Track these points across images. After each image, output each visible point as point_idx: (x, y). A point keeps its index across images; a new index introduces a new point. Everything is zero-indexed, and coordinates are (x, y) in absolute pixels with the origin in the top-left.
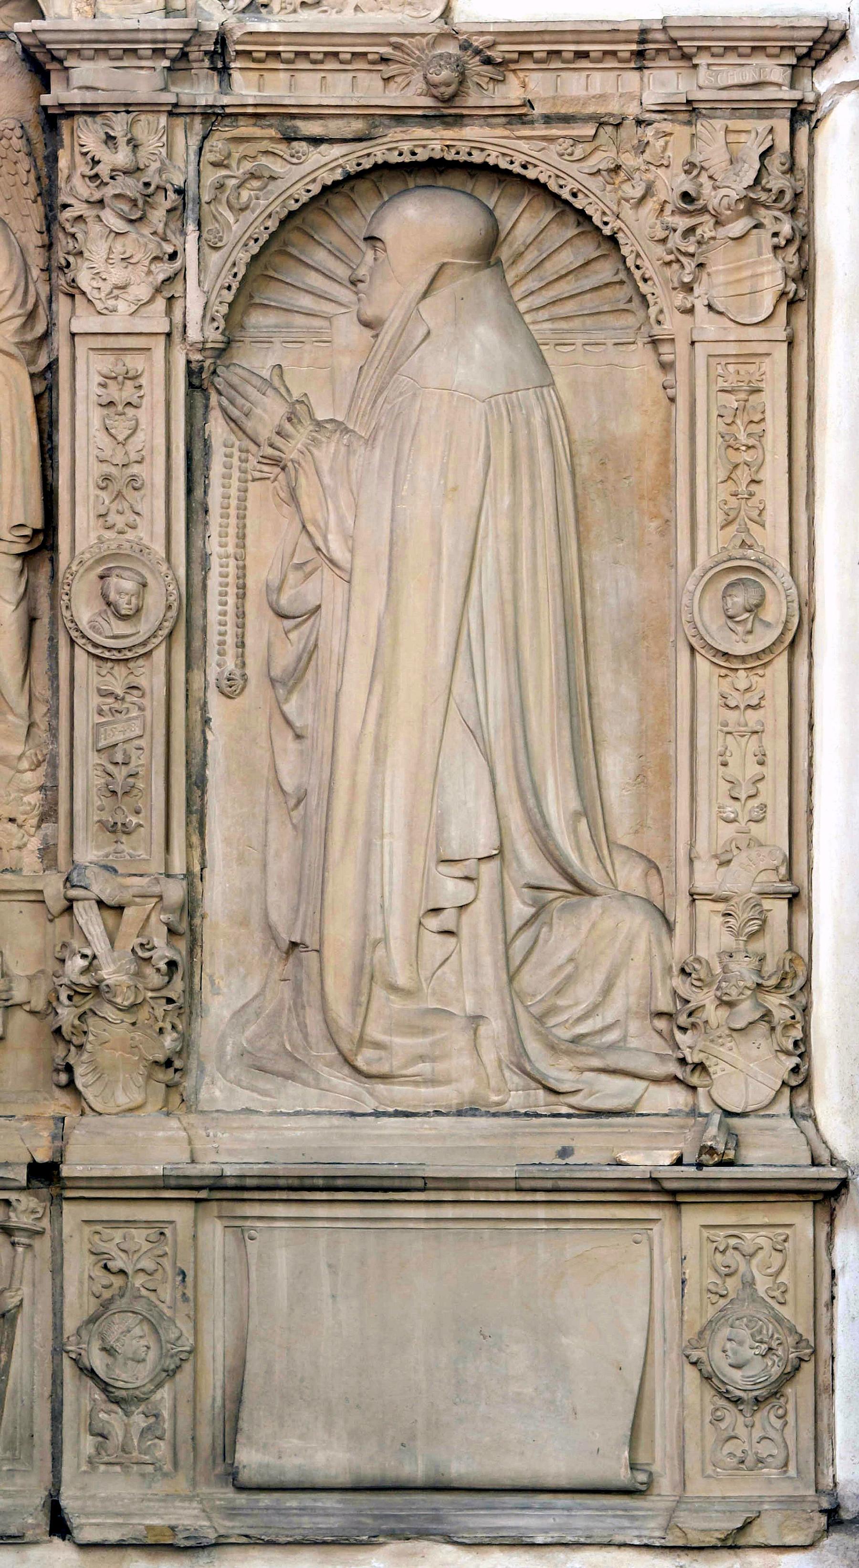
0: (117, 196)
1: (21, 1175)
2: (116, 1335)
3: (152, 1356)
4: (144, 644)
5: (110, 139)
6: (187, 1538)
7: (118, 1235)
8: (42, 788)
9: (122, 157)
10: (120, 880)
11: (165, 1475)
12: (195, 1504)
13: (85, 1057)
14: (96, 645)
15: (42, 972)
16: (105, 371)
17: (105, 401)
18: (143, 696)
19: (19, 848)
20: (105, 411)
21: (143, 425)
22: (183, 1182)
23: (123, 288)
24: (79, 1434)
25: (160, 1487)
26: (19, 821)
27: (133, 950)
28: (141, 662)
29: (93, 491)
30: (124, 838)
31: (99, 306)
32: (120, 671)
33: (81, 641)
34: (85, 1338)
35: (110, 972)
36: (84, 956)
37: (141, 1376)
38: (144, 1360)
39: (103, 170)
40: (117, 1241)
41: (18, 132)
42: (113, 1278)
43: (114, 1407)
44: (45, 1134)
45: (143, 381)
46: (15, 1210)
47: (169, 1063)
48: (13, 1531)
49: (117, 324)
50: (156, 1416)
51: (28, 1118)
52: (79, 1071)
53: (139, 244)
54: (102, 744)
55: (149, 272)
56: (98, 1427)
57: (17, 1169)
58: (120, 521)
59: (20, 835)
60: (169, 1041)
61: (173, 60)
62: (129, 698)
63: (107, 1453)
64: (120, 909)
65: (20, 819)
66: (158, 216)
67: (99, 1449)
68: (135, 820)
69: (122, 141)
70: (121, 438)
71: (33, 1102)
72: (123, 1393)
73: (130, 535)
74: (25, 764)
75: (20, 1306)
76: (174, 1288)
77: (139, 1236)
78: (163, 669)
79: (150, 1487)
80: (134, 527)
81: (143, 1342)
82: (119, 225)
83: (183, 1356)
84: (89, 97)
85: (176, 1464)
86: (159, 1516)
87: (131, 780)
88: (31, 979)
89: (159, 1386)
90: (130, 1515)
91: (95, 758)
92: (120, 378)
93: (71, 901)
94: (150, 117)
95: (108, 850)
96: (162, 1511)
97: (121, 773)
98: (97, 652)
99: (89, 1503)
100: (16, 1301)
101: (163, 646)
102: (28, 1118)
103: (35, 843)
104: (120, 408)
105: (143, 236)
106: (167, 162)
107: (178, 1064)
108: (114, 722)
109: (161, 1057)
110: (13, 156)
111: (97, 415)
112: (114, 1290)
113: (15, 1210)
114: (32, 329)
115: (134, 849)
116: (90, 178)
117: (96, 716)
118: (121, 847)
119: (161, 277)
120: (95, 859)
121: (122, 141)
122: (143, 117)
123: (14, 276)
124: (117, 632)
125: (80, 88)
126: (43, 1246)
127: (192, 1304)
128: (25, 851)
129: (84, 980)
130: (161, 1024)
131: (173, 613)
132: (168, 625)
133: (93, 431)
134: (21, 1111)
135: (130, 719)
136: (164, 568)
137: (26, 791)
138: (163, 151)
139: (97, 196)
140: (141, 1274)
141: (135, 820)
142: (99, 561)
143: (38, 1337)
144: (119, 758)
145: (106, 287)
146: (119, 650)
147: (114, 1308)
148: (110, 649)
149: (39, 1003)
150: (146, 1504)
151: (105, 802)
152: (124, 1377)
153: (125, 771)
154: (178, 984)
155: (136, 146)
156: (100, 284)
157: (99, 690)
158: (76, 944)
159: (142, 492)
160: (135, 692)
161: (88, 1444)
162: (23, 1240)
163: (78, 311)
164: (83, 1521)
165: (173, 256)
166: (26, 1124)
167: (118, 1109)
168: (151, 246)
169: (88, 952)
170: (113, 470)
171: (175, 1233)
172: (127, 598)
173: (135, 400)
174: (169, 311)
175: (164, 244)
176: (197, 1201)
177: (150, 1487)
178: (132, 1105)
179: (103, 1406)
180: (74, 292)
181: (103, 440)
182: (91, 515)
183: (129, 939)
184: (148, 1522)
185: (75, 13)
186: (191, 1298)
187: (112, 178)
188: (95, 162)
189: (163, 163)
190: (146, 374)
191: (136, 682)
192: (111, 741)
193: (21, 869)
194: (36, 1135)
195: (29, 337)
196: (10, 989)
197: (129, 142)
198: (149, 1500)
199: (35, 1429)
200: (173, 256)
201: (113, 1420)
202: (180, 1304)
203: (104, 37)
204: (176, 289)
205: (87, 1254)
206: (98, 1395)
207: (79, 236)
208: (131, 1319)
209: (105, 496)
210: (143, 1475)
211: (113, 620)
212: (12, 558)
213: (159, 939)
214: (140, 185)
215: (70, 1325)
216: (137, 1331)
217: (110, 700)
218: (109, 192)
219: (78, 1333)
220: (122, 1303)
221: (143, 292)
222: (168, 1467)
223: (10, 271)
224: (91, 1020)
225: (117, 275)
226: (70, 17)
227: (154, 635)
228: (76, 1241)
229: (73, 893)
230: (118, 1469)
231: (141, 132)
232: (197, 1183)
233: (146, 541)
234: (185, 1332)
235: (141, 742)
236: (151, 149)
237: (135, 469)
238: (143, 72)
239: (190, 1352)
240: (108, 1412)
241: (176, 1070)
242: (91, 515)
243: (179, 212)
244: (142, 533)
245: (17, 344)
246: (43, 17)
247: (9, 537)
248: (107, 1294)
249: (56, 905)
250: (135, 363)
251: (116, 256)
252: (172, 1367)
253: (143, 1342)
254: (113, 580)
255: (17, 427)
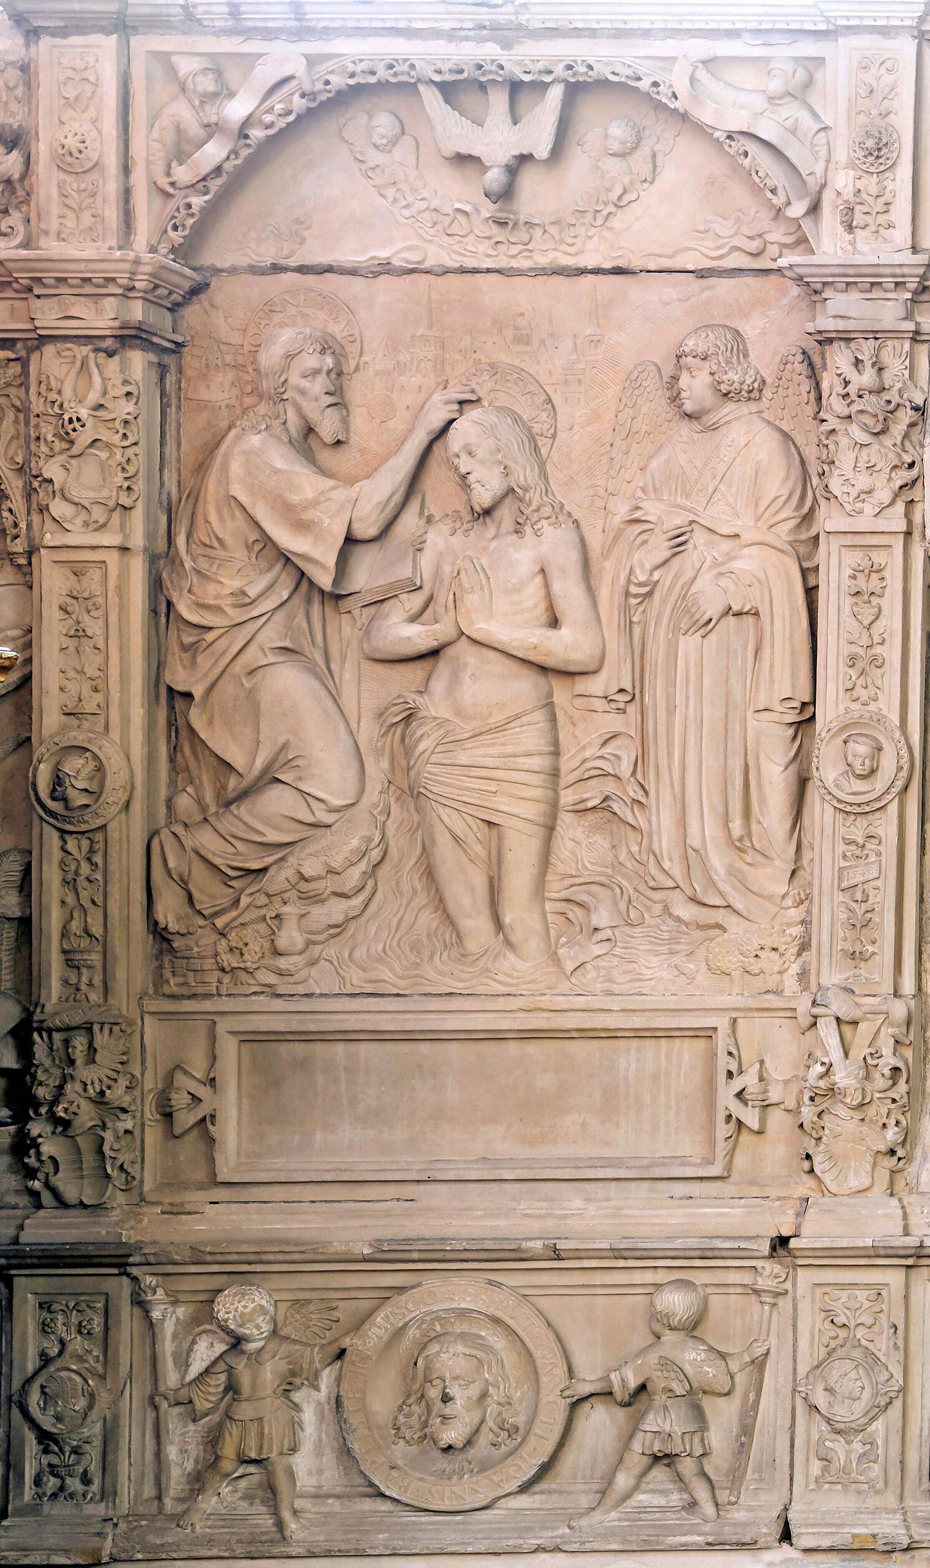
0: (862, 412)
1: (766, 1248)
2: (836, 1378)
3: (866, 1395)
4: (878, 799)
5: (858, 362)
6: (885, 1544)
7: (844, 1295)
8: (802, 922)
9: (867, 378)
10: (856, 999)
11: (877, 1492)
12: (898, 1516)
13: (822, 1147)
14: (839, 801)
15: (795, 1076)
16: (855, 565)
17: (853, 592)
18: (880, 844)
19: (780, 973)
20: (855, 600)
21: (885, 612)
22: (890, 1252)
23: (870, 492)
24: (808, 1459)
25: (873, 1502)
26: (781, 950)
27: (865, 1058)
28: (878, 815)
29: (843, 669)
30: (862, 964)
31: (848, 508)
32: (862, 822)
33: (828, 797)
34: (811, 1380)
35: (843, 1077)
36: (823, 1064)
37: (856, 1412)
38: (859, 1398)
39: (852, 389)
40: (843, 1300)
41: (800, 357)
42: (838, 1330)
43: (838, 1437)
44: (791, 1212)
45: (886, 574)
46: (761, 1275)
47: (892, 1152)
48: (747, 1539)
49: (864, 523)
50: (871, 1443)
51: (779, 1199)
52: (817, 1160)
53: (881, 453)
54: (845, 885)
55: (890, 479)
56: (822, 1453)
57: (760, 1241)
58: (864, 695)
59: (781, 962)
60: (892, 1135)
61: (915, 293)
62: (868, 846)
63: (832, 1475)
64: (855, 1023)
65: (782, 948)
66: (898, 430)
67: (825, 1469)
68: (871, 949)
69: (868, 364)
70: (866, 623)
71: (787, 1185)
72: (842, 1426)
73: (873, 707)
74: (789, 902)
75: (767, 1354)
76: (889, 1339)
77: (862, 1295)
78: (895, 821)
79: (864, 1502)
80: (876, 700)
81: (859, 1383)
82: (864, 438)
83: (893, 1395)
84: (841, 325)
85: (886, 1483)
86: (865, 1525)
87: (868, 915)
88: (786, 1082)
89: (873, 1419)
90: (843, 1525)
91: (840, 897)
92: (866, 571)
93: (816, 1017)
94: (896, 342)
95: (850, 974)
96: (869, 1522)
97: (860, 909)
98: (841, 806)
99: (811, 1515)
100: (762, 1350)
101: (896, 800)
102: (779, 1199)
103: (795, 969)
104: (866, 597)
105: (885, 447)
106: (909, 383)
107: (900, 1153)
108: (855, 866)
109: (883, 1148)
110: (796, 379)
111: (848, 602)
112: (840, 1341)
113: (761, 1275)
114: (808, 530)
115: (870, 974)
116: (843, 396)
117: (841, 861)
118: (858, 971)
119: (899, 483)
120: (836, 981)
121: (868, 364)
122: (889, 343)
123: (790, 484)
124: (855, 789)
125: (835, 317)
126: (785, 1304)
127: (902, 1352)
128: (785, 976)
129: (822, 1084)
130: (885, 1120)
131: (904, 773)
132: (900, 784)
133: (843, 617)
134: (774, 1193)
135: (868, 864)
136: (897, 734)
137: (789, 925)
138: (906, 373)
139: (846, 412)
140: (861, 1327)
141: (871, 949)
142: (843, 729)
143: (781, 1379)
144: (859, 896)
145: (854, 494)
146: (859, 805)
147: (835, 1356)
148: (851, 804)
149: (792, 1105)
150: (858, 1516)
151: (849, 934)
152: (841, 1412)
153: (864, 907)
154: (902, 1087)
155: (880, 369)
156: (850, 489)
157: (844, 839)
158: (818, 1053)
159: (883, 670)
160: (873, 840)
161: (816, 1467)
162: (768, 1300)
163: (833, 514)
164: (803, 1531)
165: (912, 465)
166: (777, 1203)
167: (850, 1191)
168: (891, 455)
169: (826, 1060)
170: (861, 651)
171: (889, 1294)
172: (861, 760)
173: (878, 591)
174: (908, 515)
175: (903, 454)
176: (908, 1267)
177: (864, 1502)
178: (860, 1188)
179: (828, 1436)
180: (830, 496)
181: (850, 623)
182: (841, 689)
183: (860, 1050)
184: (856, 1531)
185: (839, 252)
186: (902, 1347)
187: (860, 397)
188: (847, 383)
189: (904, 383)
190: (888, 567)
191: (872, 831)
192: (853, 882)
193: (782, 991)
194: (784, 1213)
195: (803, 537)
196: (766, 1091)
197: (874, 364)
198: (861, 1513)
199: (777, 1454)
200: (912, 465)
201: (838, 1446)
202: (892, 1352)
203: (851, 271)
204: (915, 494)
205: (818, 1311)
206: (824, 1427)
207: (831, 447)
208: (848, 1365)
209: (854, 673)
210: (859, 1492)
211: (852, 779)
212: (785, 727)
213: (887, 1049)
214: (883, 403)
215: (802, 1369)
216: (853, 1375)
217: (853, 848)
218: (855, 408)
219: (807, 1377)
220: (841, 1352)
221: (884, 495)
222: (880, 1485)
223: (787, 478)
224: (826, 1117)
225: (863, 481)
226: (836, 253)
227: (887, 792)
228: (808, 1300)
229: (816, 1011)
230: (839, 1487)
231: (887, 357)
232: (901, 1252)
233: (884, 712)
234: (896, 1376)
235: (878, 883)
236: (895, 371)
237: (878, 650)
238: (889, 303)
239: (899, 1392)
240: (832, 1441)
241: (900, 1159)
242: (841, 689)
243: (919, 427)
244: (882, 704)
245: (791, 543)
246: (813, 252)
247: (780, 708)
248: (833, 1344)
249: (806, 1021)
250: (879, 558)
251: (862, 465)
252: (883, 1403)
253: (859, 1383)
254: (851, 745)
255: (787, 614)
